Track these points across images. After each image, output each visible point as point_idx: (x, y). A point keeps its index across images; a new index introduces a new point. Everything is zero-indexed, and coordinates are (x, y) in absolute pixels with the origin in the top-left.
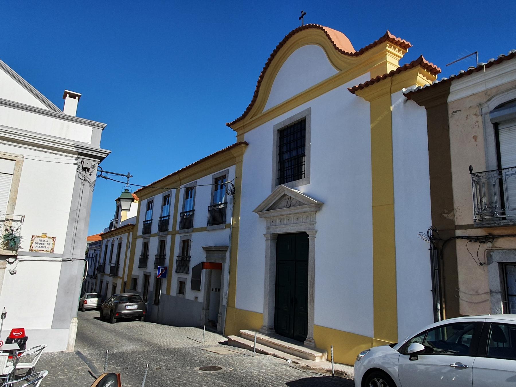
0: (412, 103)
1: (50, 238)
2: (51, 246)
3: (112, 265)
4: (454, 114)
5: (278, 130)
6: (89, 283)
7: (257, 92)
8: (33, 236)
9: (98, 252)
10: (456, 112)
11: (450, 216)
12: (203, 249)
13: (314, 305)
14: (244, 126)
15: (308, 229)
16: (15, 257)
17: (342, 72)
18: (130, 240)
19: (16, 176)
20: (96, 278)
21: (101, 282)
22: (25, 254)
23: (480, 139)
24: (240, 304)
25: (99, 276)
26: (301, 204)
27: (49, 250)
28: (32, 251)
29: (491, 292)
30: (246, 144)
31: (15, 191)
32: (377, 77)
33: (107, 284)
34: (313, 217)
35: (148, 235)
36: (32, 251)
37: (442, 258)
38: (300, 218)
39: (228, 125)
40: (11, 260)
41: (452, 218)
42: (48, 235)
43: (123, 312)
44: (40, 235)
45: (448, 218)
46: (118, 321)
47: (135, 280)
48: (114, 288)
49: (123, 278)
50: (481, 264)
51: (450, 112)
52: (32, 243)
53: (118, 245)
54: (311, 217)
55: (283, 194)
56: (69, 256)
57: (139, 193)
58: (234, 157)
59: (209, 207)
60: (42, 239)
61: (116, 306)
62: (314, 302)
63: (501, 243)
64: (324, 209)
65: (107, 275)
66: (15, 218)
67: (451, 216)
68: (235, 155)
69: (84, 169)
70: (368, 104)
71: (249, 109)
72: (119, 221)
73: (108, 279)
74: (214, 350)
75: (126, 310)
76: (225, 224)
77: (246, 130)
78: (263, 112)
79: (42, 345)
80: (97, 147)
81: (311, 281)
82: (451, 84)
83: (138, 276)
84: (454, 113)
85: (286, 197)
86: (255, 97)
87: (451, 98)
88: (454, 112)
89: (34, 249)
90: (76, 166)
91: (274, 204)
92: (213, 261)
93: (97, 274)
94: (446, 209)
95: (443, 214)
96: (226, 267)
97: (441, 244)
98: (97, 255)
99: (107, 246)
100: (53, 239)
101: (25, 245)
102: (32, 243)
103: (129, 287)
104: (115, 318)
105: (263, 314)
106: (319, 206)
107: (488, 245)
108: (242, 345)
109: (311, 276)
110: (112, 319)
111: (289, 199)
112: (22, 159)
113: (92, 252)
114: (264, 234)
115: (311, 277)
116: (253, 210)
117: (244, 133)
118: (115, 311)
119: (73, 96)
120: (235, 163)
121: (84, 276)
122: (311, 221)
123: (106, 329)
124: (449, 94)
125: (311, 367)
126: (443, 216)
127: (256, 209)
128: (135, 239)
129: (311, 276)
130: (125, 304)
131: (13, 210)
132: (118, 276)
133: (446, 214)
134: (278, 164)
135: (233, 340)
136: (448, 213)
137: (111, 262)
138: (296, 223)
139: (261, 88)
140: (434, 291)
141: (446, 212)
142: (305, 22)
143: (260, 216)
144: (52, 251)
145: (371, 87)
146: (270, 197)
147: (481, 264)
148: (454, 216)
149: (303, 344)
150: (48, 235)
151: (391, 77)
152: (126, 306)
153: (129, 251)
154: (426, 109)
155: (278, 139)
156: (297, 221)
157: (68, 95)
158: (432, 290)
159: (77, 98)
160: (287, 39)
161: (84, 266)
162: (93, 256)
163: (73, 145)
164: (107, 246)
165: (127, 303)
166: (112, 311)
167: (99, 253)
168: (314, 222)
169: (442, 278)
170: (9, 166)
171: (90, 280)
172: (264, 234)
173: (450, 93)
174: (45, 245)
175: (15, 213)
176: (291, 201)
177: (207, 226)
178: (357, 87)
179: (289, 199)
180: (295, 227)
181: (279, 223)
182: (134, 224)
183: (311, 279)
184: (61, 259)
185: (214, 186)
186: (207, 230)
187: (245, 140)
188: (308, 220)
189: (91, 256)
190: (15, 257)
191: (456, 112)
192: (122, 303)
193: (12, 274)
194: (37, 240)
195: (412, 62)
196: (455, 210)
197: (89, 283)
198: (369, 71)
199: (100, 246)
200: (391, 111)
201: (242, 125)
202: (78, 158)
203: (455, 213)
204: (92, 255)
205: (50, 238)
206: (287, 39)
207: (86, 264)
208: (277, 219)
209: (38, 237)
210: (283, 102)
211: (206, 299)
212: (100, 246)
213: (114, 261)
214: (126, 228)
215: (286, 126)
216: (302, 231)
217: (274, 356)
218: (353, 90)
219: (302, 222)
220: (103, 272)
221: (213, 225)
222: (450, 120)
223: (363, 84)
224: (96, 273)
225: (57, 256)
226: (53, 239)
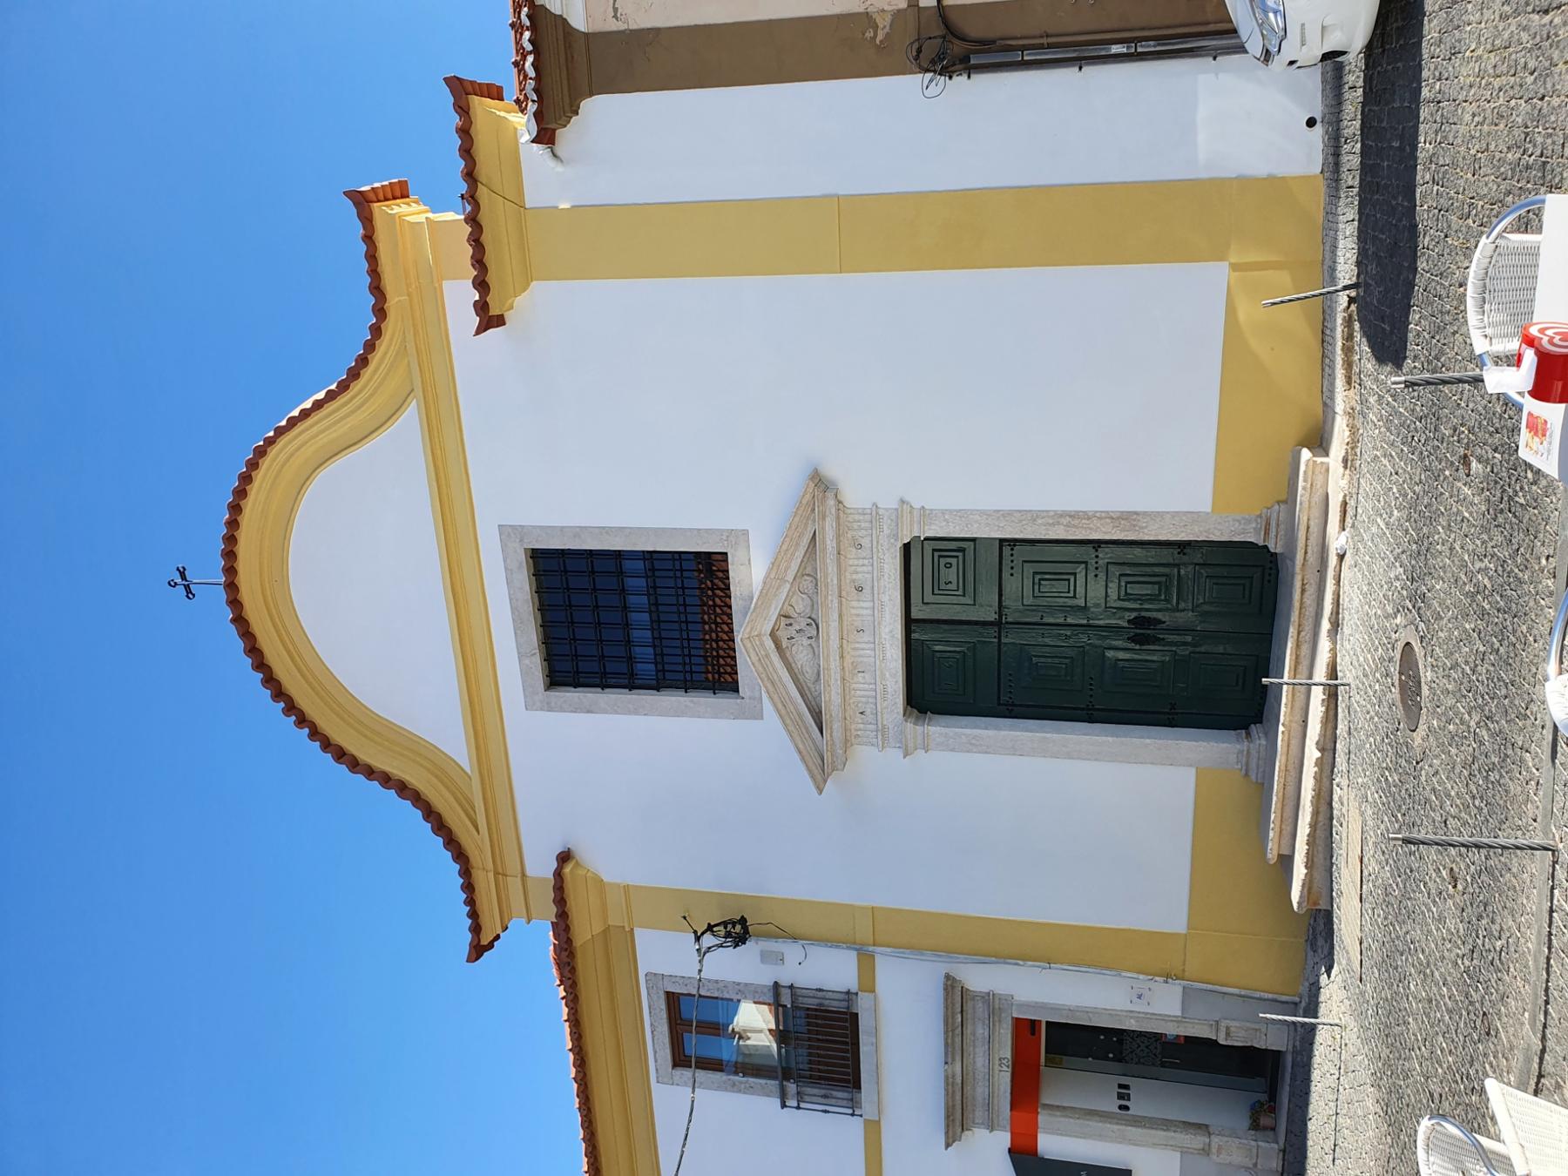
0: (564, 136)
4: (621, 15)
7: (386, 780)
10: (615, 10)
11: (884, 22)
12: (954, 1141)
13: (1145, 514)
14: (496, 873)
15: (892, 541)
17: (419, 392)
26: (808, 570)
32: (467, 223)
34: (857, 517)
37: (993, 42)
38: (854, 576)
39: (478, 950)
41: (888, 18)
45: (888, 27)
51: (614, 26)
54: (855, 526)
55: (769, 644)
58: (606, 931)
59: (784, 1106)
62: (1136, 513)
64: (832, 471)
67: (884, 19)
68: (598, 929)
71: (440, 826)
74: (1353, 893)
76: (857, 994)
77: (512, 866)
78: (469, 772)
81: (1067, 526)
82: (542, 6)
84: (619, 15)
85: (783, 634)
87: (579, 22)
88: (615, 17)
94: (864, 35)
95: (878, 42)
97: (957, 47)
105: (1197, 768)
106: (820, 485)
108: (1321, 818)
109: (1050, 525)
111: (791, 625)
114: (904, 757)
115: (1053, 524)
116: (814, 790)
117: (523, 875)
120: (627, 929)
122: (867, 525)
124: (565, 19)
125: (1346, 441)
126: (881, 42)
127: (813, 777)
129: (1050, 525)
133: (876, 35)
134: (663, 693)
135: (1306, 867)
136: (876, 27)
138: (873, 681)
139: (379, 763)
140: (1080, 62)
141: (872, 34)
142: (209, 571)
145: (490, 259)
148: (883, 11)
149: (1282, 554)
151: (479, 184)
154: (591, 96)
155: (577, 689)
156: (867, 590)
158: (1077, 69)
160: (240, 621)
168: (874, 514)
169: (1044, 41)
172: (904, 757)
173: (565, 16)
176: (796, 615)
177: (861, 1116)
178: (480, 297)
179: (791, 625)
180: (885, 598)
181: (867, 676)
183: (1058, 523)
185: (701, 1075)
186: (877, 1119)
188: (866, 542)
191: (615, 10)
195: (456, 107)
196: (869, 10)
198: (441, 286)
201: (491, 875)
203: (875, 10)
206: (240, 621)
208: (854, 649)
211: (1164, 1130)
215: (539, 645)
216: (898, 568)
217: (1337, 634)
218: (489, 320)
219: (870, 568)
221: (859, 1088)
222: (633, 26)
223: (476, 273)
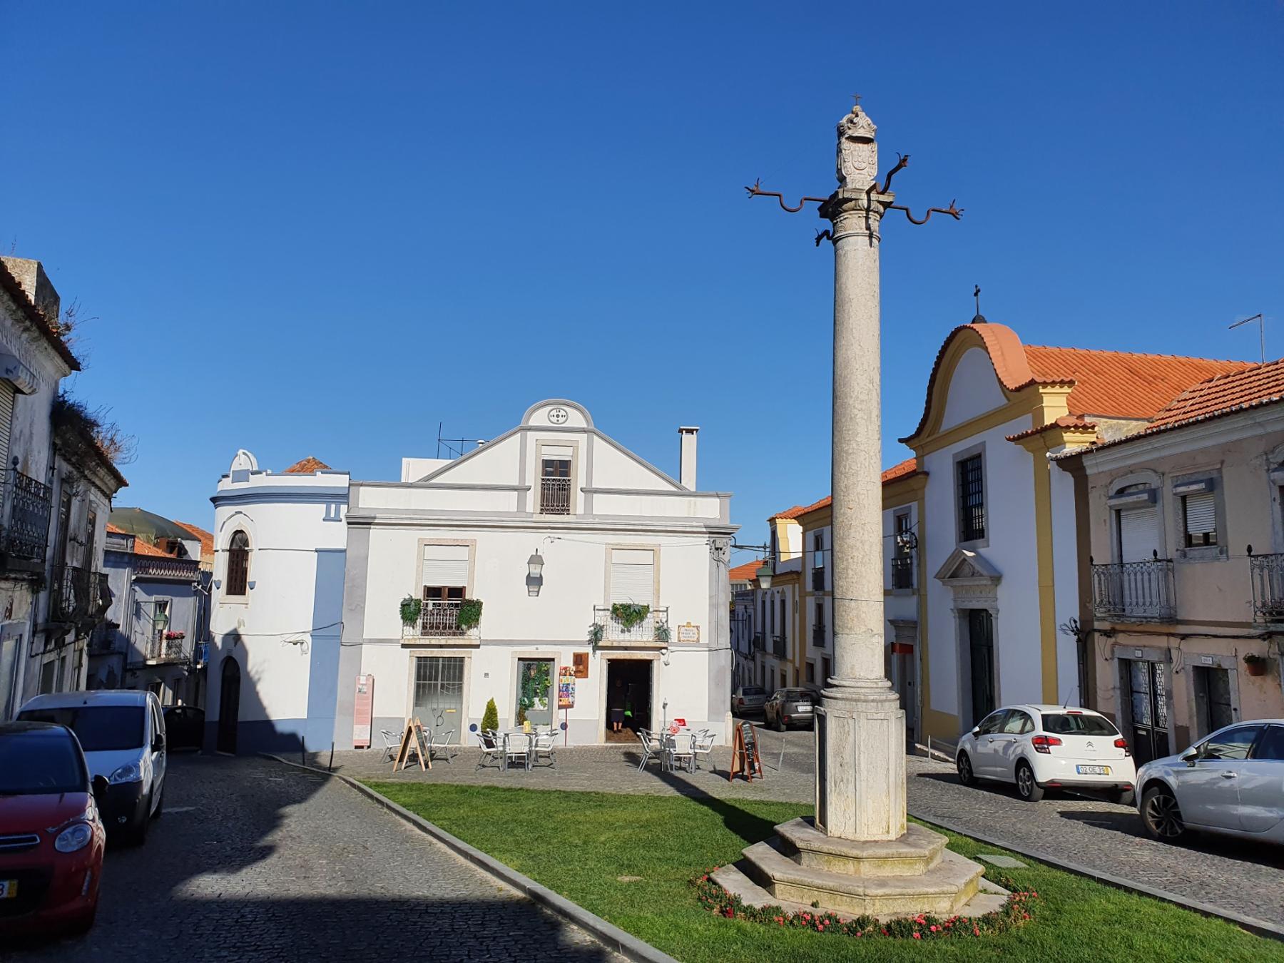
1: (694, 627)
2: (696, 636)
3: (775, 639)
5: (958, 463)
6: (743, 668)
8: (679, 626)
9: (751, 611)
16: (666, 648)
18: (797, 598)
19: (655, 564)
20: (753, 659)
21: (763, 668)
22: (674, 645)
23: (1108, 521)
24: (935, 705)
25: (758, 655)
27: (695, 639)
28: (680, 641)
29: (1114, 688)
30: (927, 474)
31: (657, 582)
33: (773, 671)
35: (821, 593)
36: (680, 641)
39: (901, 441)
40: (664, 651)
42: (692, 624)
43: (793, 715)
44: (685, 624)
46: (788, 729)
47: (811, 667)
48: (784, 677)
49: (793, 662)
50: (1106, 659)
51: (1090, 487)
52: (679, 633)
53: (781, 604)
56: (714, 646)
57: (800, 518)
60: (688, 629)
61: (783, 706)
63: (1121, 638)
65: (770, 654)
66: (661, 609)
69: (717, 549)
70: (1031, 455)
72: (777, 559)
73: (772, 661)
75: (798, 712)
79: (706, 729)
80: (727, 523)
83: (815, 660)
86: (928, 409)
89: (682, 639)
90: (708, 546)
91: (956, 569)
92: (904, 642)
93: (754, 652)
96: (917, 650)
98: (750, 616)
99: (764, 602)
100: (697, 627)
101: (674, 637)
102: (679, 633)
103: (803, 678)
104: (784, 724)
107: (1112, 640)
110: (780, 726)
112: (658, 548)
113: (740, 608)
118: (783, 713)
119: (690, 431)
121: (732, 667)
123: (772, 737)
128: (803, 595)
130: (795, 704)
131: (658, 602)
132: (786, 658)
137: (773, 633)
143: (944, 584)
144: (698, 640)
146: (949, 561)
147: (1106, 659)
150: (692, 624)
152: (797, 706)
153: (797, 616)
157: (684, 432)
159: (695, 432)
161: (730, 656)
162: (745, 618)
163: (704, 530)
164: (764, 602)
165: (798, 701)
166: (778, 713)
167: (753, 613)
170: (647, 557)
171: (745, 662)
174: (691, 634)
175: (661, 604)
182: (799, 569)
184: (707, 649)
187: (926, 470)
189: (740, 618)
190: (666, 648)
192: (792, 701)
193: (666, 665)
194: (682, 630)
197: (743, 668)
199: (752, 600)
200: (1049, 470)
202: (709, 537)
204: (743, 615)
205: (694, 627)
207: (732, 653)
209: (684, 626)
210: (956, 426)
212: (752, 600)
213: (778, 632)
214: (789, 577)
220: (764, 649)
224: (752, 651)
225: (703, 645)
226: (697, 627)
